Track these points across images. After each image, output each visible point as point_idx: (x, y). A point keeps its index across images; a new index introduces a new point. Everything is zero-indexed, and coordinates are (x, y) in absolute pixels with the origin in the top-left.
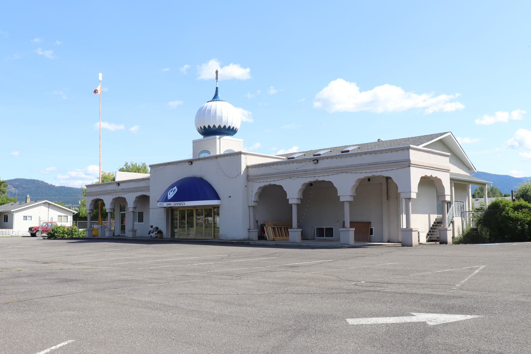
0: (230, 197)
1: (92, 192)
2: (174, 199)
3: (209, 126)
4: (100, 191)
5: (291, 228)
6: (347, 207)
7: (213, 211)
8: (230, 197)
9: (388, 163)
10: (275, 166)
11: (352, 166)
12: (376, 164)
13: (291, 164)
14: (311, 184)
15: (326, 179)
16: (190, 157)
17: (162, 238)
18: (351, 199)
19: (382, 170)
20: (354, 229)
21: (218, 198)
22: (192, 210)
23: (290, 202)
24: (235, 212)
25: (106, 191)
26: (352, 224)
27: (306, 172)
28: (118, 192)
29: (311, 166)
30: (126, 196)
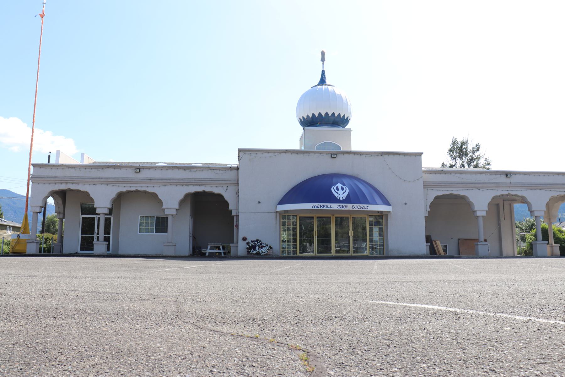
1: (55, 177)
2: (348, 200)
4: (78, 178)
7: (380, 219)
8: (406, 204)
10: (458, 175)
11: (545, 184)
15: (462, 193)
18: (484, 214)
24: (408, 221)
25: (99, 178)
27: (498, 185)
29: (131, 174)
30: (161, 192)
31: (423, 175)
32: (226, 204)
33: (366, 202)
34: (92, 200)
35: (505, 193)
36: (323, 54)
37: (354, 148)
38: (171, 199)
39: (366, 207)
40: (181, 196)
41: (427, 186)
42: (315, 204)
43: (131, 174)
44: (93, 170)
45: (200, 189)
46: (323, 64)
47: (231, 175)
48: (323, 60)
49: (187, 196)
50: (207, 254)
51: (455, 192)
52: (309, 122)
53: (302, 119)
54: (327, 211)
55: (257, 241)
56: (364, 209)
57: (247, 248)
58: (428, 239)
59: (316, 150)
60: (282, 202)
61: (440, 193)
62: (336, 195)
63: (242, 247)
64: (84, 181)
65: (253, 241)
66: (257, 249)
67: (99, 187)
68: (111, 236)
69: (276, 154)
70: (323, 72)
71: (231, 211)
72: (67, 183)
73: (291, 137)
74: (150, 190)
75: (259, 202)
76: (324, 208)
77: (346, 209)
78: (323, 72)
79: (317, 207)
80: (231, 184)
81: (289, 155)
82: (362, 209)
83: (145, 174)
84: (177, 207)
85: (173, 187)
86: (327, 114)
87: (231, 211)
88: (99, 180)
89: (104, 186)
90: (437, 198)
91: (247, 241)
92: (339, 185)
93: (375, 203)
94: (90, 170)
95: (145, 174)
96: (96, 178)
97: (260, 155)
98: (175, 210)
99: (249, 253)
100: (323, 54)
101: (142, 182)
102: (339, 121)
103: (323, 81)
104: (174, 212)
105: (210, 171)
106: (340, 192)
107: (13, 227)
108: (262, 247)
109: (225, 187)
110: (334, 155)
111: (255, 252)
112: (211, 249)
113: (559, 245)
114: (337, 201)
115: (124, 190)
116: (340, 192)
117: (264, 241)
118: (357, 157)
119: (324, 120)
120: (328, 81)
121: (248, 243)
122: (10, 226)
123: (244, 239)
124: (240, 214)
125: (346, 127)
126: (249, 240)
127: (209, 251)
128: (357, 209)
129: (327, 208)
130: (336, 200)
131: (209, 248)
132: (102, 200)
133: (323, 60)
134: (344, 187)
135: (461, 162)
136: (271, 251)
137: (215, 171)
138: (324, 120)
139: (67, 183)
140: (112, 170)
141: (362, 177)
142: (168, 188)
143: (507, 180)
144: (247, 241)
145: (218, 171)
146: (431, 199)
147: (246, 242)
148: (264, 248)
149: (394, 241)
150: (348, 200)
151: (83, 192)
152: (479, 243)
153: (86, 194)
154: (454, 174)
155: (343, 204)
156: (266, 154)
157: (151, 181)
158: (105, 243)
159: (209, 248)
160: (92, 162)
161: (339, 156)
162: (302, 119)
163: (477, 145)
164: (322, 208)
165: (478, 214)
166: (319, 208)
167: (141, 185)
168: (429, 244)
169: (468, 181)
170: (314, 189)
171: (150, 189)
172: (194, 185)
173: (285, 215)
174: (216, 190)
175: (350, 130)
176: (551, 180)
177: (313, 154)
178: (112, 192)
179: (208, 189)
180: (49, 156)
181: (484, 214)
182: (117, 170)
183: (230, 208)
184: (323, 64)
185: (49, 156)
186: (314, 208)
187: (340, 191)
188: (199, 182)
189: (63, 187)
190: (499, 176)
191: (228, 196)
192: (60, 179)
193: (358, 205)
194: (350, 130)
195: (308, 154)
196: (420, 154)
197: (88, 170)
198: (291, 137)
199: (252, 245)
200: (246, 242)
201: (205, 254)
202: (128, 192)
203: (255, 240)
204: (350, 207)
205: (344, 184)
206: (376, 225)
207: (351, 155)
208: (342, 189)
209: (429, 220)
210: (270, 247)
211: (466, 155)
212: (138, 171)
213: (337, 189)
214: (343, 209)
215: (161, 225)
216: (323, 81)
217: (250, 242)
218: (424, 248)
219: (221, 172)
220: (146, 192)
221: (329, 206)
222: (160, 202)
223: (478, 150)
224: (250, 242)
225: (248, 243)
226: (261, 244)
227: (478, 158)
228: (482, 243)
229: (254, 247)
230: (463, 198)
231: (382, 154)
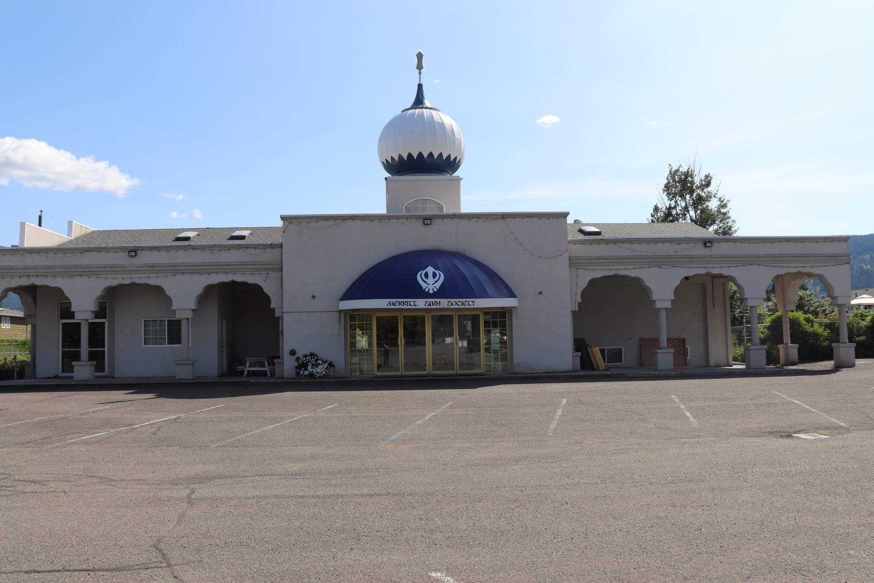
0: (541, 293)
1: (11, 268)
2: (441, 293)
3: (420, 154)
4: (46, 267)
5: (838, 342)
6: (663, 316)
7: (500, 319)
8: (541, 293)
9: (821, 256)
10: (627, 245)
11: (767, 256)
12: (803, 256)
13: (181, 253)
14: (687, 278)
15: (633, 273)
16: (382, 210)
17: (708, 366)
18: (668, 305)
19: (603, 268)
20: (797, 345)
21: (512, 295)
22: (396, 318)
23: (659, 305)
24: (546, 321)
25: (77, 266)
26: (669, 340)
27: (690, 259)
28: (131, 272)
29: (122, 259)
30: (170, 284)
31: (572, 246)
32: (267, 299)
33: (472, 294)
34: (68, 299)
35: (702, 271)
36: (420, 56)
37: (465, 209)
38: (184, 292)
39: (471, 303)
40: (199, 290)
41: (575, 263)
42: (391, 300)
43: (122, 259)
44: (67, 255)
45: (226, 278)
46: (420, 73)
47: (269, 256)
48: (420, 67)
49: (209, 289)
50: (246, 373)
51: (622, 273)
52: (402, 167)
53: (390, 161)
54: (424, 304)
55: (312, 355)
56: (467, 307)
57: (296, 367)
58: (580, 345)
59: (404, 213)
60: (347, 296)
61: (599, 274)
62: (424, 285)
63: (288, 365)
64: (55, 271)
65: (305, 356)
66: (309, 367)
67: (77, 279)
68: (106, 349)
69: (338, 222)
70: (420, 86)
71: (274, 310)
72: (29, 276)
73: (366, 192)
74: (152, 282)
75: (313, 297)
76: (405, 307)
77: (438, 307)
78: (420, 86)
79: (394, 304)
80: (273, 270)
81: (357, 223)
82: (463, 307)
83: (144, 259)
84: (194, 308)
85: (187, 276)
86: (420, 155)
87: (274, 310)
88: (75, 270)
89: (84, 279)
90: (593, 282)
91: (296, 356)
92: (430, 270)
93: (486, 295)
94: (62, 255)
95: (144, 259)
96: (72, 266)
97: (313, 224)
98: (191, 312)
99: (298, 374)
100: (420, 56)
101: (142, 269)
102: (443, 165)
103: (419, 101)
104: (190, 315)
105: (241, 250)
106: (431, 280)
107: (12, 318)
108: (317, 365)
109: (264, 274)
110: (427, 220)
111: (307, 373)
112: (250, 366)
113: (797, 345)
114: (424, 294)
115: (114, 283)
116: (431, 280)
117: (322, 354)
118: (464, 222)
119: (421, 164)
120: (427, 103)
121: (298, 359)
122: (6, 317)
123: (293, 353)
124: (285, 316)
125: (455, 174)
126: (300, 354)
127: (247, 368)
128: (456, 307)
129: (409, 307)
130: (422, 294)
131: (248, 364)
132: (83, 300)
133: (420, 67)
134: (437, 272)
135: (683, 204)
136: (331, 370)
137: (249, 250)
138: (421, 164)
139: (29, 276)
140: (94, 254)
141: (473, 253)
142: (179, 277)
143: (706, 252)
144: (296, 356)
145: (252, 251)
146: (583, 284)
147: (294, 358)
148: (320, 367)
149: (526, 349)
150: (441, 293)
151: (54, 288)
152: (658, 351)
153: (58, 291)
154: (621, 244)
155: (434, 300)
156: (322, 223)
157: (153, 268)
158: (89, 363)
159: (248, 364)
160: (75, 234)
161: (437, 223)
162: (390, 161)
163: (707, 176)
164: (401, 307)
165: (659, 305)
166: (397, 307)
167: (140, 275)
168: (580, 354)
169: (643, 254)
170: (392, 276)
171: (152, 280)
172: (217, 273)
173: (352, 316)
174: (251, 279)
175: (459, 179)
176: (775, 249)
177: (395, 221)
178: (96, 287)
179: (239, 278)
180: (40, 217)
181: (668, 305)
182: (103, 255)
183: (273, 306)
184: (420, 73)
185: (40, 217)
186: (389, 307)
187: (431, 279)
188: (226, 267)
189: (25, 282)
190: (693, 245)
191: (269, 288)
192: (19, 271)
193: (457, 300)
194: (459, 179)
195: (387, 221)
196: (565, 215)
197: (59, 255)
198: (366, 192)
199: (303, 363)
200: (294, 358)
201: (242, 372)
202: (121, 286)
203: (308, 353)
204: (444, 303)
205: (437, 268)
206: (495, 326)
207: (455, 220)
208: (434, 275)
209: (577, 316)
210: (331, 365)
211: (691, 192)
212: (133, 254)
213: (426, 275)
214: (434, 307)
215: (174, 331)
216: (419, 101)
217: (301, 356)
218: (567, 359)
219: (257, 251)
220: (147, 286)
221: (412, 303)
222: (168, 300)
223: (708, 184)
224: (301, 356)
225: (298, 359)
226: (316, 360)
227: (709, 197)
228: (664, 351)
229: (304, 366)
230: (637, 283)
231: (504, 216)
